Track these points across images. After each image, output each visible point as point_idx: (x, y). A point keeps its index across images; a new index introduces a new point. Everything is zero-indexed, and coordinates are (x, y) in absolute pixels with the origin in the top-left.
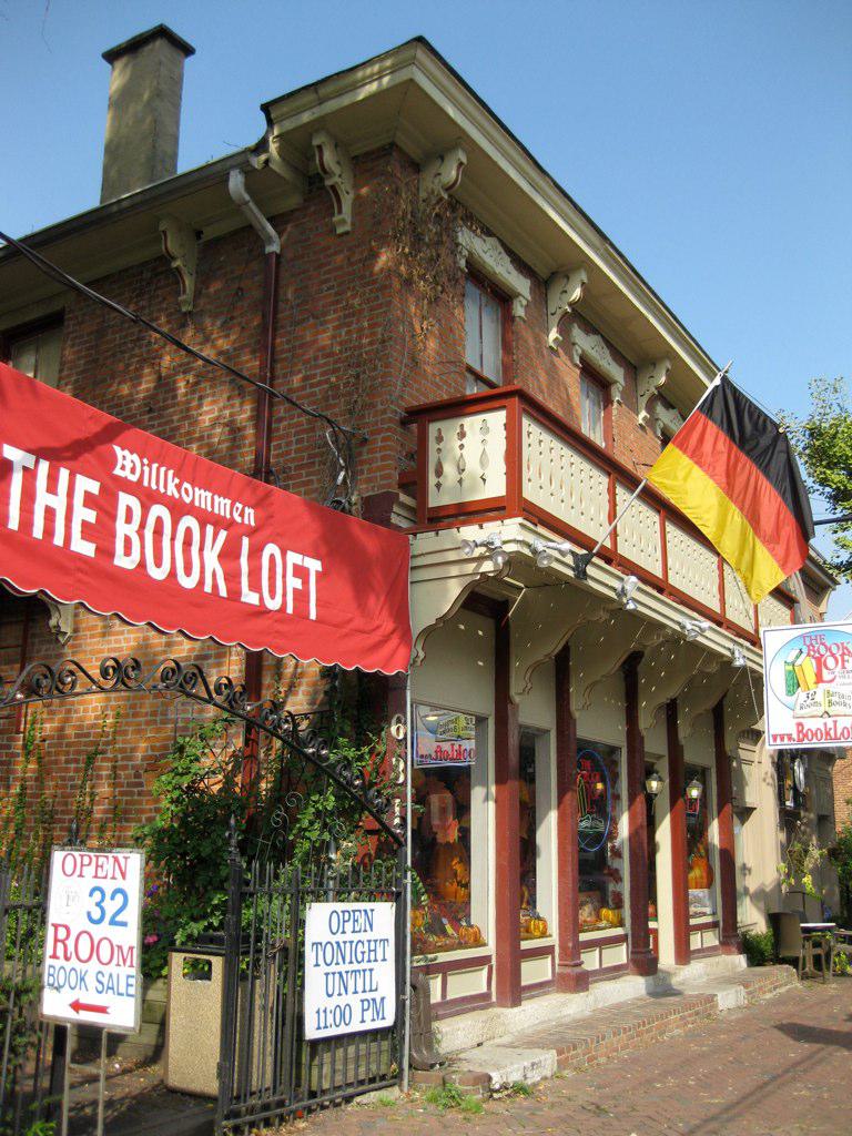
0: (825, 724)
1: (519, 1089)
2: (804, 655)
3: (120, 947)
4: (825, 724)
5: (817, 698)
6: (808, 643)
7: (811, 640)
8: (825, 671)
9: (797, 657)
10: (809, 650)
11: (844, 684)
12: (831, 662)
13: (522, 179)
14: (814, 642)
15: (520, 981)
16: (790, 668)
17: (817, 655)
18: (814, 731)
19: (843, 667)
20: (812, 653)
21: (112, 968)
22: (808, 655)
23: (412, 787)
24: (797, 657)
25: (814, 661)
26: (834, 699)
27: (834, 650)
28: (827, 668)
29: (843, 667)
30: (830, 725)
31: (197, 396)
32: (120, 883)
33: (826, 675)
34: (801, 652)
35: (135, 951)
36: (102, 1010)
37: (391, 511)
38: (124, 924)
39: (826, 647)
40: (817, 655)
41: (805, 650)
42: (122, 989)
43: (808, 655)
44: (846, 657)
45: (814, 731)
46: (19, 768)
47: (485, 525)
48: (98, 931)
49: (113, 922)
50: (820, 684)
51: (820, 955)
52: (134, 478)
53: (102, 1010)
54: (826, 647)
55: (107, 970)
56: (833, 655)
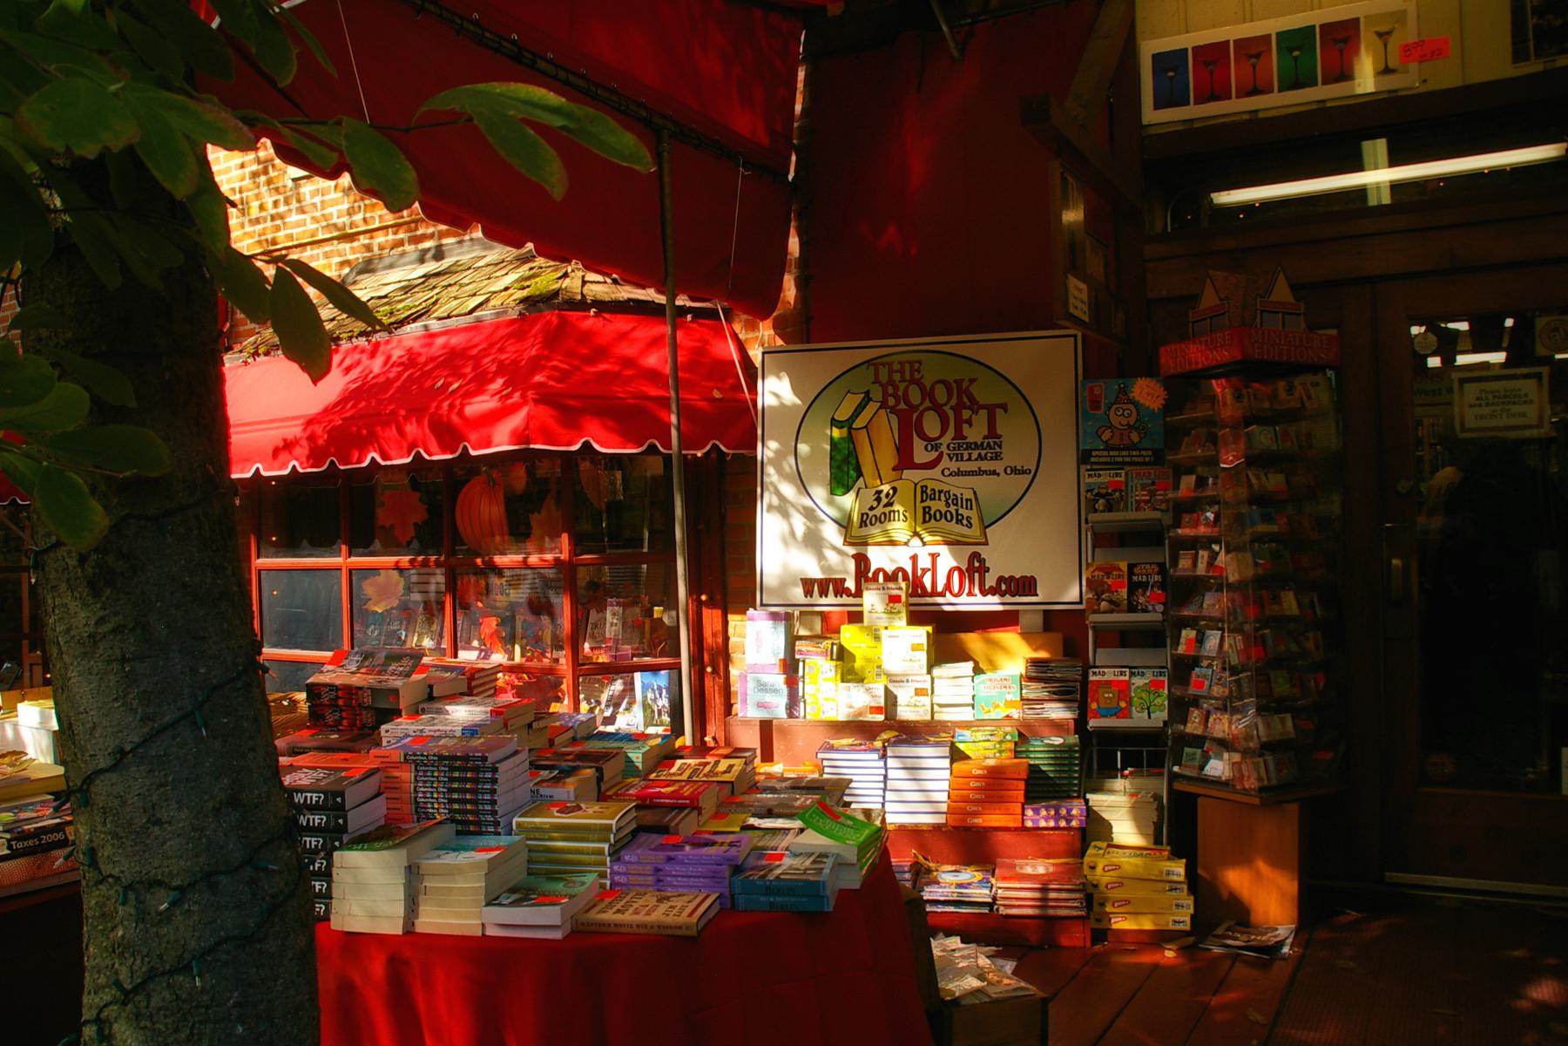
0: (914, 558)
1: (86, 388)
2: (872, 407)
4: (914, 558)
6: (884, 378)
7: (891, 372)
8: (918, 444)
10: (885, 395)
11: (959, 473)
12: (931, 425)
14: (897, 377)
17: (902, 406)
18: (878, 523)
19: (959, 435)
20: (891, 401)
22: (884, 405)
23: (35, 828)
25: (894, 419)
27: (941, 394)
28: (923, 436)
29: (959, 435)
30: (925, 562)
31: (328, 418)
33: (921, 454)
34: (867, 398)
37: (276, 754)
39: (922, 387)
40: (902, 406)
41: (877, 394)
43: (884, 405)
44: (966, 414)
45: (878, 523)
50: (907, 473)
51: (763, 760)
52: (76, 732)
54: (922, 387)
56: (937, 408)
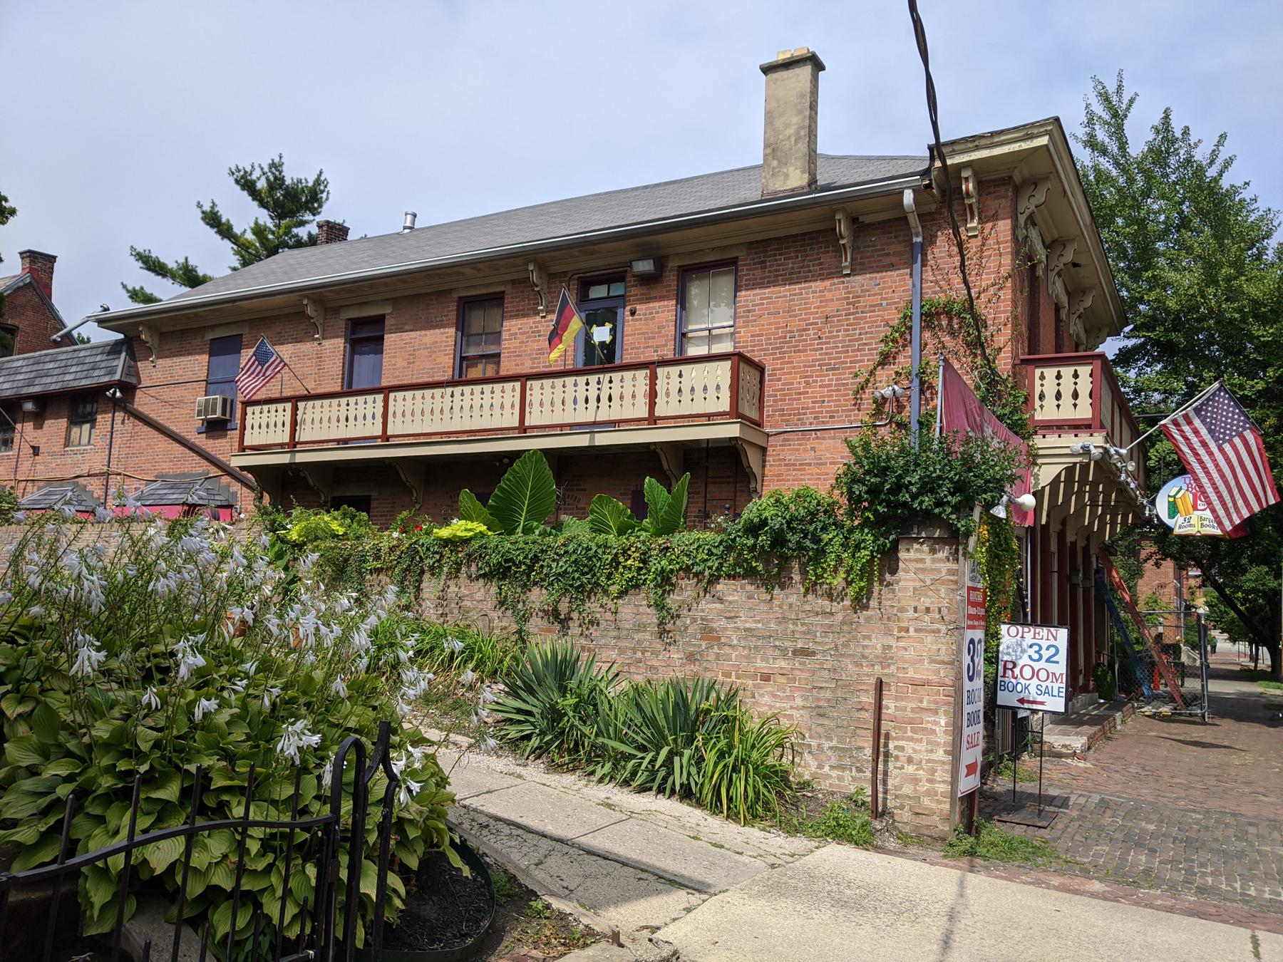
2: (1182, 492)
3: (1054, 674)
5: (1192, 522)
9: (1178, 492)
13: (972, 154)
15: (225, 890)
16: (1172, 499)
21: (1048, 683)
24: (1178, 492)
26: (1205, 523)
32: (1052, 642)
35: (1064, 676)
36: (1042, 703)
38: (1057, 662)
42: (1055, 693)
46: (292, 615)
47: (1095, 434)
48: (1037, 666)
49: (1048, 661)
53: (1042, 703)
55: (1044, 685)
